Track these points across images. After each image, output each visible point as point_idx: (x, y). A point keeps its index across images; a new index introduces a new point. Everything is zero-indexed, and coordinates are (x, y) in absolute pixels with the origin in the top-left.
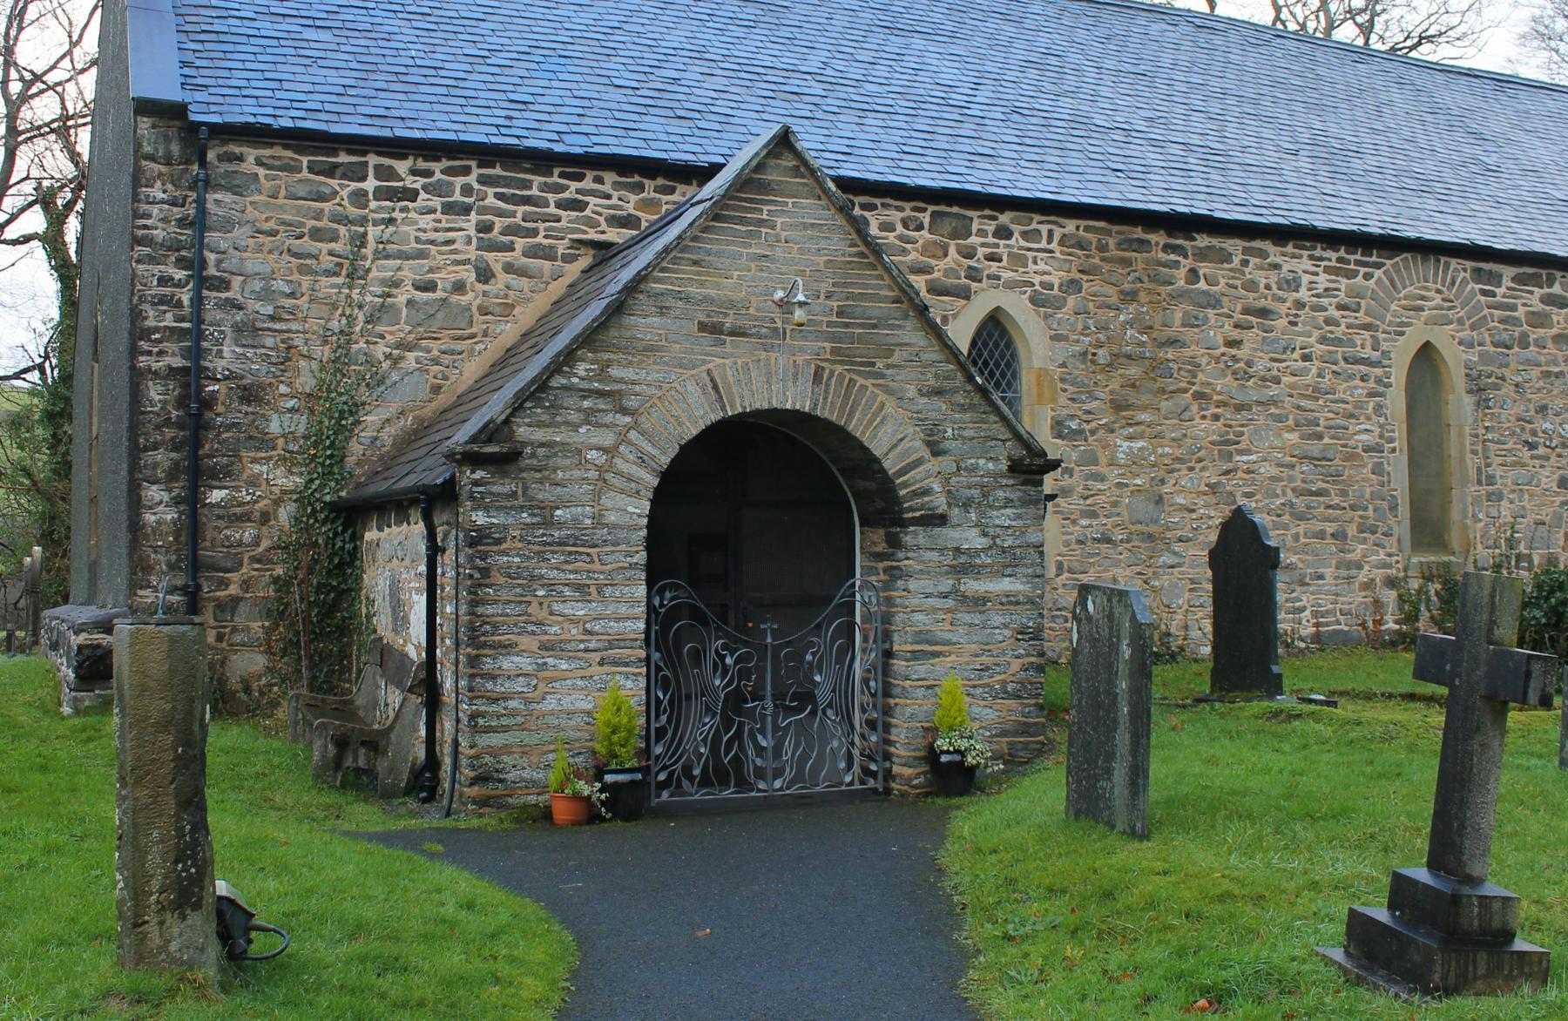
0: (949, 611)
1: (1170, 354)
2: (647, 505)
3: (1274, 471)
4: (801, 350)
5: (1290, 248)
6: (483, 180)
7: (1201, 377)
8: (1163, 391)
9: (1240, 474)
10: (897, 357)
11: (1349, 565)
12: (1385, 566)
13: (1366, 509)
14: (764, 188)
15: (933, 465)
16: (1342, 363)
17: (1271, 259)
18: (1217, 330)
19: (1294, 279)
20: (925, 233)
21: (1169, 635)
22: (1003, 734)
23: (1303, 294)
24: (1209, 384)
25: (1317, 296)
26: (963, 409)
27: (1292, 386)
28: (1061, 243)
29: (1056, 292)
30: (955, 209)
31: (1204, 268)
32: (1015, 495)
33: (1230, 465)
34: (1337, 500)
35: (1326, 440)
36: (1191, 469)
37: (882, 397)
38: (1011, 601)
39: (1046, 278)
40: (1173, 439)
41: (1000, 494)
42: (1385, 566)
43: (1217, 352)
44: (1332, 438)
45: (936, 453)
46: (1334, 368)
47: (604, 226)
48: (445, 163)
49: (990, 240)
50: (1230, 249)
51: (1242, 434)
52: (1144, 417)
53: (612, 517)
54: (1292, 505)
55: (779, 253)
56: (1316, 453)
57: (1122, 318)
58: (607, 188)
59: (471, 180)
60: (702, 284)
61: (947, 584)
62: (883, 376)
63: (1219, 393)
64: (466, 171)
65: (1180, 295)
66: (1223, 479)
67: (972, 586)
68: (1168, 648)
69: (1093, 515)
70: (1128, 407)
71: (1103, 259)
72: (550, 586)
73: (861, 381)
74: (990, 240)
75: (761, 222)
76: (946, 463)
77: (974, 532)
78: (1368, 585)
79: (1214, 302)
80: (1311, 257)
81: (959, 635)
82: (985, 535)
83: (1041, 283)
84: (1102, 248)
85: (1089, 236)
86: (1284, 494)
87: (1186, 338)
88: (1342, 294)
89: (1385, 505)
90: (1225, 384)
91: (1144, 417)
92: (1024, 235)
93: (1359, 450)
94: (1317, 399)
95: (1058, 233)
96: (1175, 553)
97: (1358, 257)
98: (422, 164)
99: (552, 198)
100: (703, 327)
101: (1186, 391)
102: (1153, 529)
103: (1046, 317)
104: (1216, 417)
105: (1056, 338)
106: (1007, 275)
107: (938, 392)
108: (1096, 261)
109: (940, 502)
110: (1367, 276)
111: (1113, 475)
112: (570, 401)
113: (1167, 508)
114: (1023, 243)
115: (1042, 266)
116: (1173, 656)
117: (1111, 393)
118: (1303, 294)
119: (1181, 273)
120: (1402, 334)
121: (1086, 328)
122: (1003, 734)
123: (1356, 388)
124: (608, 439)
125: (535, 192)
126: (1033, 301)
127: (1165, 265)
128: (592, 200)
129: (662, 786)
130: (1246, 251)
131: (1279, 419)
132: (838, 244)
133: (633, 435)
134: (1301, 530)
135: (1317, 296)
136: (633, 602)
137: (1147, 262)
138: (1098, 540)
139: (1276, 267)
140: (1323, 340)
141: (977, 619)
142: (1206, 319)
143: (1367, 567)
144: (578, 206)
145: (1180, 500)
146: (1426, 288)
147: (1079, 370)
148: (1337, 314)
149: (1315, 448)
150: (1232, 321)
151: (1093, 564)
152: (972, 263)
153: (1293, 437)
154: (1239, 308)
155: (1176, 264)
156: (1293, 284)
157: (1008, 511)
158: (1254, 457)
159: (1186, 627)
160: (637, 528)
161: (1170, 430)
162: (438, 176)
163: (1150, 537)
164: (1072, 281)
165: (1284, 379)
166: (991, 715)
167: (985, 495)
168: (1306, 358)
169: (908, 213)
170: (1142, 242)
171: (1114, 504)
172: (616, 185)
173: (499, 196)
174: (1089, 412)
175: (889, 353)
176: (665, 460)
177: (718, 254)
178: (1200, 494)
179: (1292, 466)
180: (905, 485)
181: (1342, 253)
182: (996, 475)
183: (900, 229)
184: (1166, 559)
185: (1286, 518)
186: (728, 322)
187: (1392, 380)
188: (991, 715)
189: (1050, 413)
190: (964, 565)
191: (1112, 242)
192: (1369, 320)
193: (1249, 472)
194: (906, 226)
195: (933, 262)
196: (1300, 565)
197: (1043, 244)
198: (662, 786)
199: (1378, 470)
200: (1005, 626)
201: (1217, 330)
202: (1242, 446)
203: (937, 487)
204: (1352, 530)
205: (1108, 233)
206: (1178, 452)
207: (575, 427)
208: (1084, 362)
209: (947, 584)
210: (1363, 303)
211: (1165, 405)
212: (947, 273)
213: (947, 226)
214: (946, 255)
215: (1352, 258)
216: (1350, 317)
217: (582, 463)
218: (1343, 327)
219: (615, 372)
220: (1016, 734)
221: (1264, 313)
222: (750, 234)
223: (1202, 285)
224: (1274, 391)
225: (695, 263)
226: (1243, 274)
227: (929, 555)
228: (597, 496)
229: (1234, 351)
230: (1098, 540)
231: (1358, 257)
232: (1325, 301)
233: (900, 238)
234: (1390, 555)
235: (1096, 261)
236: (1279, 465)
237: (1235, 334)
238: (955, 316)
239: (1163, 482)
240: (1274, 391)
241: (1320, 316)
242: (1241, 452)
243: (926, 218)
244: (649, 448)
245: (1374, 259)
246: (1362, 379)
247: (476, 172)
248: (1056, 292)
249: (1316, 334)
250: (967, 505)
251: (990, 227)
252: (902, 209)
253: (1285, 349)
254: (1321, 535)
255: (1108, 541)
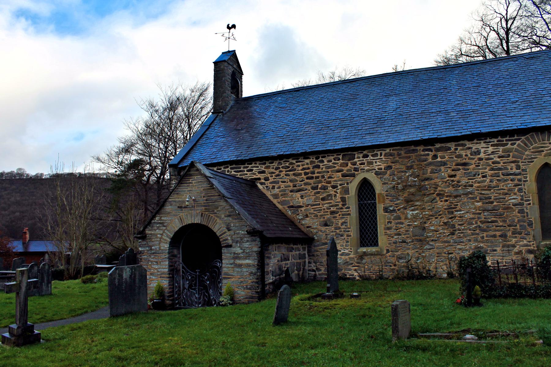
0: (232, 268)
1: (427, 183)
2: (168, 245)
3: (472, 216)
4: (198, 210)
5: (475, 141)
6: (231, 169)
7: (439, 188)
8: (425, 195)
9: (457, 218)
10: (219, 209)
11: (508, 246)
12: (527, 245)
13: (516, 226)
14: (191, 175)
15: (228, 233)
16: (502, 176)
17: (468, 146)
18: (445, 173)
19: (478, 151)
20: (341, 161)
21: (430, 270)
22: (246, 298)
23: (482, 155)
24: (442, 190)
25: (488, 155)
26: (236, 219)
27: (478, 187)
28: (385, 156)
29: (383, 170)
30: (349, 153)
31: (439, 154)
32: (249, 239)
33: (453, 215)
34: (501, 224)
35: (495, 204)
36: (436, 218)
37: (216, 218)
38: (248, 265)
39: (380, 167)
40: (429, 209)
41: (245, 239)
42: (527, 245)
43: (446, 180)
44: (498, 202)
45: (229, 230)
46: (498, 178)
47: (257, 174)
48: (224, 166)
49: (361, 159)
50: (450, 146)
51: (457, 205)
52: (417, 203)
53: (162, 248)
54: (480, 227)
55: (193, 189)
56: (490, 208)
57: (407, 174)
58: (257, 165)
59: (229, 169)
60: (178, 198)
61: (232, 261)
62: (216, 213)
63: (447, 193)
64: (228, 167)
65: (430, 164)
66: (450, 220)
67: (238, 262)
68: (430, 274)
69: (400, 235)
70: (411, 201)
71: (399, 158)
72: (151, 262)
73: (211, 215)
74: (361, 159)
75: (190, 183)
76: (232, 232)
77: (239, 249)
78: (520, 253)
79: (444, 164)
80: (485, 142)
81: (235, 274)
82: (242, 249)
83: (378, 169)
84: (399, 155)
85: (394, 152)
86: (476, 223)
87: (433, 177)
88: (501, 153)
89: (526, 224)
90: (449, 190)
91: (417, 203)
92: (372, 156)
93: (511, 206)
94: (490, 190)
95: (383, 153)
96: (431, 245)
97: (508, 138)
98: (219, 167)
99: (245, 170)
100: (179, 207)
101: (434, 194)
102: (421, 238)
103: (381, 178)
104: (446, 201)
105: (384, 184)
106: (366, 168)
107: (229, 216)
108: (397, 159)
109: (230, 242)
110: (514, 144)
111: (407, 222)
112: (155, 225)
113: (427, 231)
114: (372, 158)
115: (378, 164)
116: (432, 277)
117: (405, 197)
118: (482, 155)
119: (430, 157)
120: (532, 162)
121: (393, 179)
122: (246, 298)
123: (508, 184)
124: (161, 232)
125: (242, 169)
126: (375, 174)
127: (424, 155)
128: (254, 168)
129: (177, 304)
130: (456, 145)
131: (473, 198)
132: (206, 185)
133: (166, 231)
134: (485, 235)
135: (488, 155)
136: (166, 265)
137: (416, 156)
138: (401, 242)
139: (469, 148)
140: (492, 169)
141: (240, 270)
142: (440, 170)
143: (518, 246)
144: (251, 170)
145: (432, 228)
146: (544, 144)
147: (392, 192)
148: (498, 160)
149: (490, 207)
150: (451, 169)
151: (400, 249)
152: (355, 166)
153: (479, 204)
154: (454, 164)
155: (428, 155)
156: (479, 152)
157: (248, 243)
158: (463, 212)
159: (436, 268)
160: (166, 250)
161: (428, 206)
162: (223, 169)
163: (420, 240)
164: (388, 166)
165: (475, 185)
166: (243, 293)
167: (241, 240)
168: (483, 177)
169: (335, 156)
170: (413, 150)
171: (407, 231)
172: (260, 164)
173: (234, 171)
174: (397, 204)
175: (218, 208)
176: (172, 236)
177: (182, 191)
178: (440, 226)
179: (480, 214)
180: (221, 238)
181: (499, 138)
182: (244, 234)
183: (333, 161)
184: (427, 247)
185: (478, 231)
186: (183, 206)
187: (528, 179)
188: (243, 293)
189: (383, 206)
190: (236, 257)
191: (402, 152)
192: (514, 159)
193: (460, 217)
194: (335, 160)
195: (343, 168)
196: (485, 247)
197: (379, 157)
198: (177, 304)
199: (521, 211)
200: (247, 272)
201: (445, 173)
202: (458, 209)
203: (229, 238)
204: (509, 234)
205: (401, 150)
206: (431, 213)
207: (155, 230)
208: (394, 189)
209: (232, 261)
210: (511, 154)
211: (426, 199)
212: (347, 171)
213: (347, 158)
214: (347, 166)
215: (504, 139)
216: (505, 159)
217: (157, 237)
218: (502, 164)
219: (163, 218)
220: (250, 298)
221: (465, 164)
222: (188, 186)
223: (439, 159)
224: (470, 189)
225: (177, 194)
226: (456, 153)
227: (227, 254)
228: (160, 243)
229: (452, 179)
230: (401, 242)
231: (508, 138)
232: (492, 156)
233: (333, 163)
234: (529, 242)
235: (397, 159)
236: (473, 214)
237: (453, 173)
238: (351, 182)
239: (425, 223)
240: (470, 189)
241: (490, 162)
242: (457, 211)
243: (341, 157)
244: (169, 234)
245: (516, 137)
246: (511, 180)
247: (230, 167)
248: (383, 170)
249: (488, 168)
250: (237, 242)
251: (361, 155)
252: (333, 156)
253: (475, 175)
254: (494, 236)
255: (405, 242)
